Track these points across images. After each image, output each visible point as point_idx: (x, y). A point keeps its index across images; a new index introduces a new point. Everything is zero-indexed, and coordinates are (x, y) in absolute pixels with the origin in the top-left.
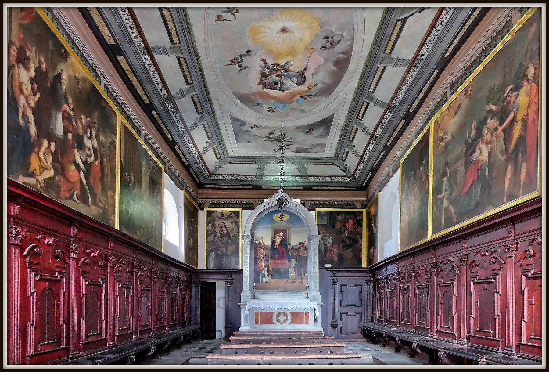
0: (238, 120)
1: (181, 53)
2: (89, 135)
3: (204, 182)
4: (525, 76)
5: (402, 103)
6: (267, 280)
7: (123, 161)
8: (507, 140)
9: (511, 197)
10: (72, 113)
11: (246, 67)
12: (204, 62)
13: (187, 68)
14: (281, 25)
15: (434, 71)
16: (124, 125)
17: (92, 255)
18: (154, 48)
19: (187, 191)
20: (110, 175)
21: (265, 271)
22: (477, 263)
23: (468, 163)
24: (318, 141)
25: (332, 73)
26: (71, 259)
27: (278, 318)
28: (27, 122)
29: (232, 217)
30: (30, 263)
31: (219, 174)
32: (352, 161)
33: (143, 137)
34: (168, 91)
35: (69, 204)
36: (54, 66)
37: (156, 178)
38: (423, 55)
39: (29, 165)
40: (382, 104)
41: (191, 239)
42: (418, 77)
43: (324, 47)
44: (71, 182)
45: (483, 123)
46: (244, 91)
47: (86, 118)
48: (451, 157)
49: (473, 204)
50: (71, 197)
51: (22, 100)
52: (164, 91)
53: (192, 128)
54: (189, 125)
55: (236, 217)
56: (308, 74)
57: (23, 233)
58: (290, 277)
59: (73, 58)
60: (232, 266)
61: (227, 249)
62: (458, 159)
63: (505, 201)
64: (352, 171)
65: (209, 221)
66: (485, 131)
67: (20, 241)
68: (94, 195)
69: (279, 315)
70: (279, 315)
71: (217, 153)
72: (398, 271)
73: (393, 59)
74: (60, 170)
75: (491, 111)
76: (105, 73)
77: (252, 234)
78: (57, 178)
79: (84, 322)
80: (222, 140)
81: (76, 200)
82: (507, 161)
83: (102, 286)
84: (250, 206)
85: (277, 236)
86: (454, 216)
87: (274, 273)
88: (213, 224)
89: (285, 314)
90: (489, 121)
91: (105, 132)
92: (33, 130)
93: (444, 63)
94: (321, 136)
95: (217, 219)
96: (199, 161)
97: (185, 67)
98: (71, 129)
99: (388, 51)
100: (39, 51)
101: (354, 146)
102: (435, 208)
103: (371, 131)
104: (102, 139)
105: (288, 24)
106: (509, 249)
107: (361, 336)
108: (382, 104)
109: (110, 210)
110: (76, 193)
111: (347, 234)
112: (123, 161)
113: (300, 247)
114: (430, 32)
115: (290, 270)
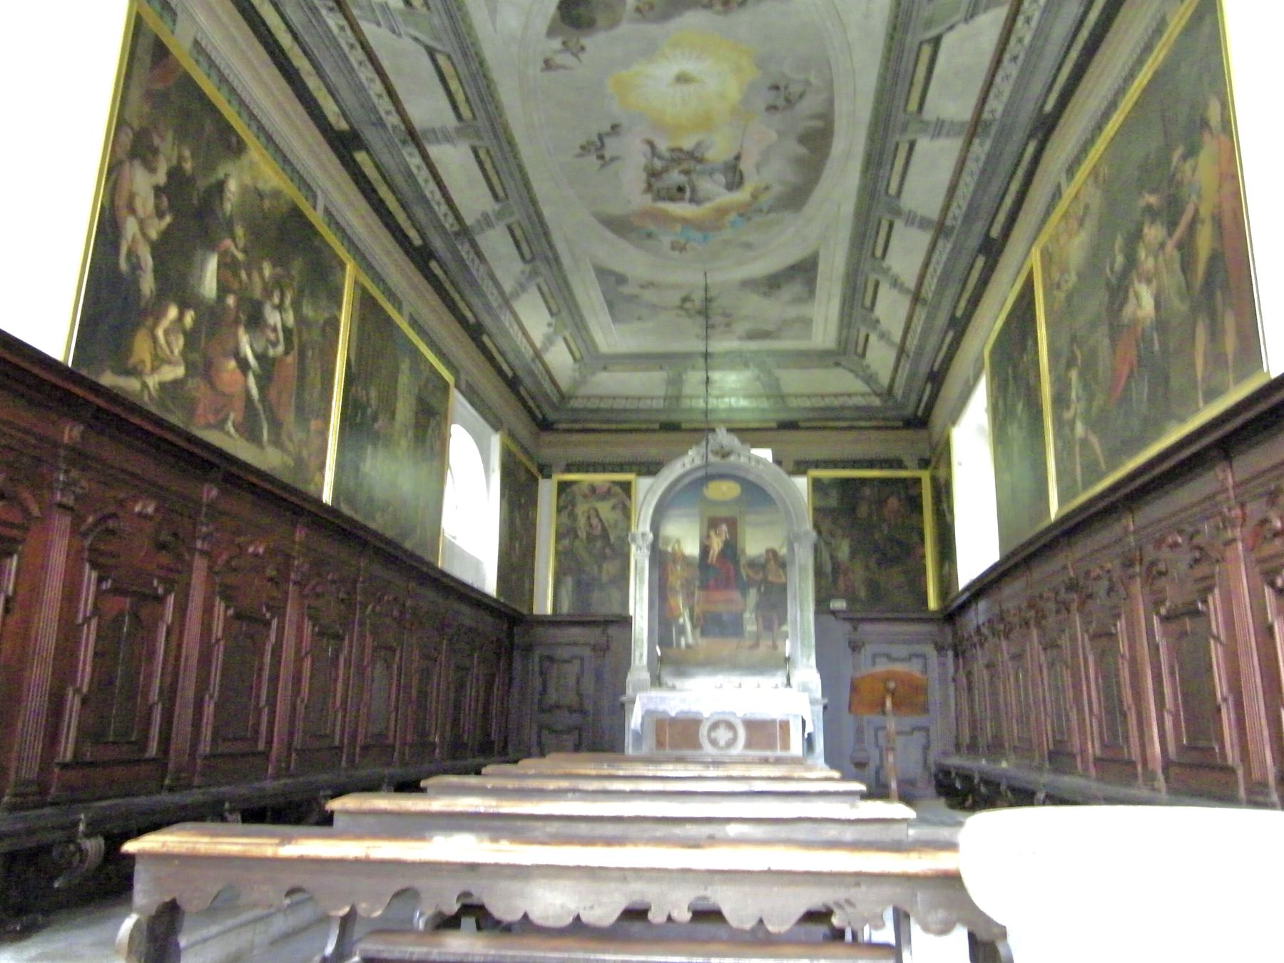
0: (611, 273)
1: (481, 138)
2: (276, 300)
3: (552, 415)
4: (1205, 124)
5: (969, 217)
6: (690, 640)
7: (353, 363)
8: (1187, 265)
9: (1212, 394)
10: (240, 256)
11: (613, 159)
12: (526, 152)
13: (494, 167)
14: (674, 69)
15: (1026, 144)
16: (364, 290)
17: (251, 550)
18: (425, 132)
19: (511, 435)
20: (319, 386)
21: (685, 620)
22: (1162, 567)
23: (1117, 329)
24: (793, 312)
25: (799, 161)
26: (197, 555)
27: (713, 735)
28: (136, 267)
29: (615, 495)
30: (92, 549)
31: (583, 397)
32: (880, 358)
33: (407, 317)
34: (458, 217)
35: (213, 437)
36: (210, 167)
37: (434, 402)
38: (992, 112)
39: (129, 351)
40: (923, 223)
41: (517, 545)
42: (993, 159)
43: (772, 108)
44: (224, 394)
45: (1135, 237)
46: (616, 209)
47: (274, 266)
48: (1082, 320)
49: (1136, 424)
50: (220, 425)
51: (131, 227)
52: (451, 219)
53: (516, 295)
54: (508, 287)
55: (625, 497)
56: (746, 166)
57: (84, 483)
58: (747, 635)
59: (255, 151)
60: (616, 609)
61: (600, 571)
62: (1093, 326)
63: (1201, 404)
64: (885, 379)
65: (562, 504)
66: (1142, 254)
67: (76, 499)
68: (276, 424)
69: (715, 726)
70: (715, 726)
71: (574, 349)
72: (1002, 612)
73: (927, 124)
74: (201, 367)
75: (1149, 209)
76: (328, 185)
77: (655, 527)
78: (191, 383)
79: (212, 706)
80: (581, 317)
81: (232, 431)
82: (1194, 310)
83: (267, 624)
84: (650, 468)
85: (712, 534)
86: (1101, 459)
87: (710, 624)
88: (572, 510)
89: (730, 726)
90: (1146, 230)
91: (313, 294)
92: (148, 284)
93: (1046, 127)
94: (798, 300)
95: (579, 498)
96: (537, 368)
97: (488, 166)
98: (236, 286)
99: (913, 106)
100: (182, 134)
101: (878, 321)
102: (1060, 445)
103: (911, 283)
104: (308, 311)
105: (690, 67)
106: (1228, 523)
107: (932, 790)
108: (923, 223)
109: (313, 464)
110: (232, 416)
111: (886, 532)
112: (353, 358)
113: (767, 561)
114: (997, 62)
115: (747, 615)
